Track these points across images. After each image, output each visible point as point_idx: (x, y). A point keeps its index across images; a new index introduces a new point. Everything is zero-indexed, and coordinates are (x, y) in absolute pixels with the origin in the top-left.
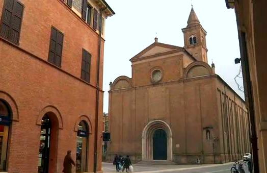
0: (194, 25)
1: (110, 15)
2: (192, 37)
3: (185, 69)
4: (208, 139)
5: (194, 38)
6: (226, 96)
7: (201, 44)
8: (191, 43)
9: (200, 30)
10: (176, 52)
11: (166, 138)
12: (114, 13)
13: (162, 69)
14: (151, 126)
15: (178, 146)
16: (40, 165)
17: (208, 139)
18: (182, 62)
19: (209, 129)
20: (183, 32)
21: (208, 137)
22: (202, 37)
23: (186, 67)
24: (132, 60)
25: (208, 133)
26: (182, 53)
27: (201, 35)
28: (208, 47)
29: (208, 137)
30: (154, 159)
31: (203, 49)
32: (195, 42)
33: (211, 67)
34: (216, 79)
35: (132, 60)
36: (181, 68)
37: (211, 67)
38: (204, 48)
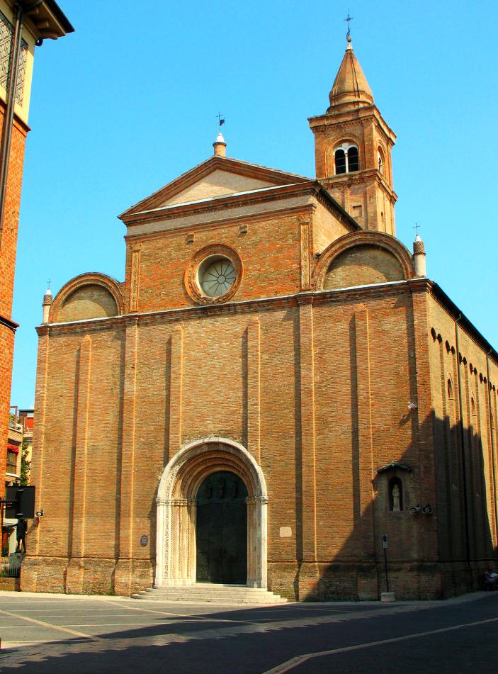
0: (353, 108)
1: (54, 33)
2: (345, 148)
3: (318, 256)
4: (397, 509)
5: (353, 152)
6: (462, 360)
7: (374, 175)
8: (340, 169)
9: (373, 125)
10: (284, 195)
11: (244, 508)
12: (69, 29)
13: (234, 253)
14: (190, 460)
15: (321, 523)
16: (279, 596)
17: (397, 509)
18: (311, 235)
19: (399, 475)
20: (315, 129)
21: (396, 501)
22: (380, 149)
23: (323, 248)
24: (130, 219)
25: (396, 493)
26: (313, 200)
27: (376, 145)
28: (395, 188)
29: (396, 501)
30: (200, 578)
31: (380, 194)
32: (354, 167)
33: (411, 251)
34: (429, 300)
35: (130, 219)
36: (305, 253)
37: (411, 251)
38: (384, 189)
